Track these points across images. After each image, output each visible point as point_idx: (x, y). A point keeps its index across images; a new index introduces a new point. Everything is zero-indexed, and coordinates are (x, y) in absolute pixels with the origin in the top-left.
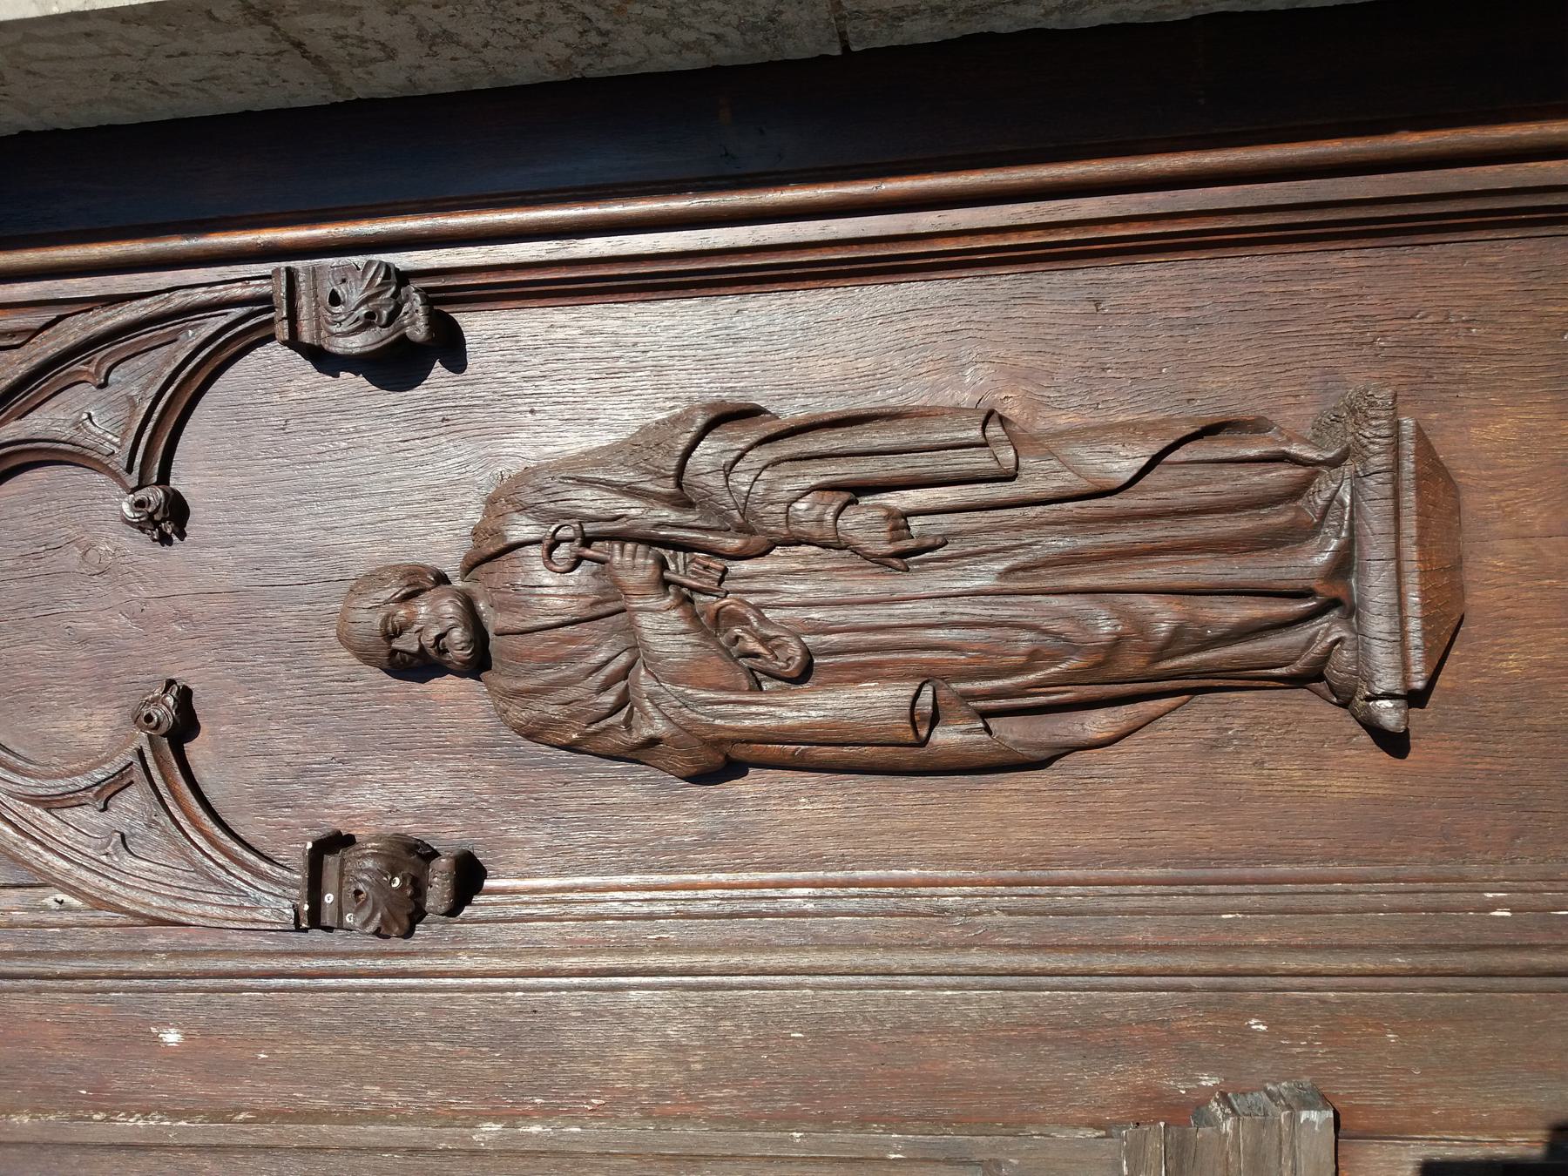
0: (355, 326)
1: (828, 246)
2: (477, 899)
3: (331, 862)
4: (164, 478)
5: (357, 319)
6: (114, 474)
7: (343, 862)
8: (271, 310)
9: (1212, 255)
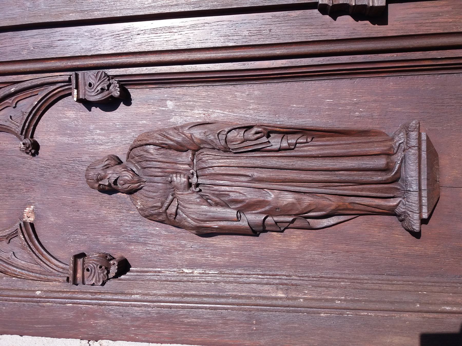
0: (97, 93)
1: (431, 60)
2: (128, 273)
3: (80, 261)
4: (32, 137)
5: (98, 91)
6: (16, 134)
7: (84, 261)
8: (71, 85)
9: (281, 81)
